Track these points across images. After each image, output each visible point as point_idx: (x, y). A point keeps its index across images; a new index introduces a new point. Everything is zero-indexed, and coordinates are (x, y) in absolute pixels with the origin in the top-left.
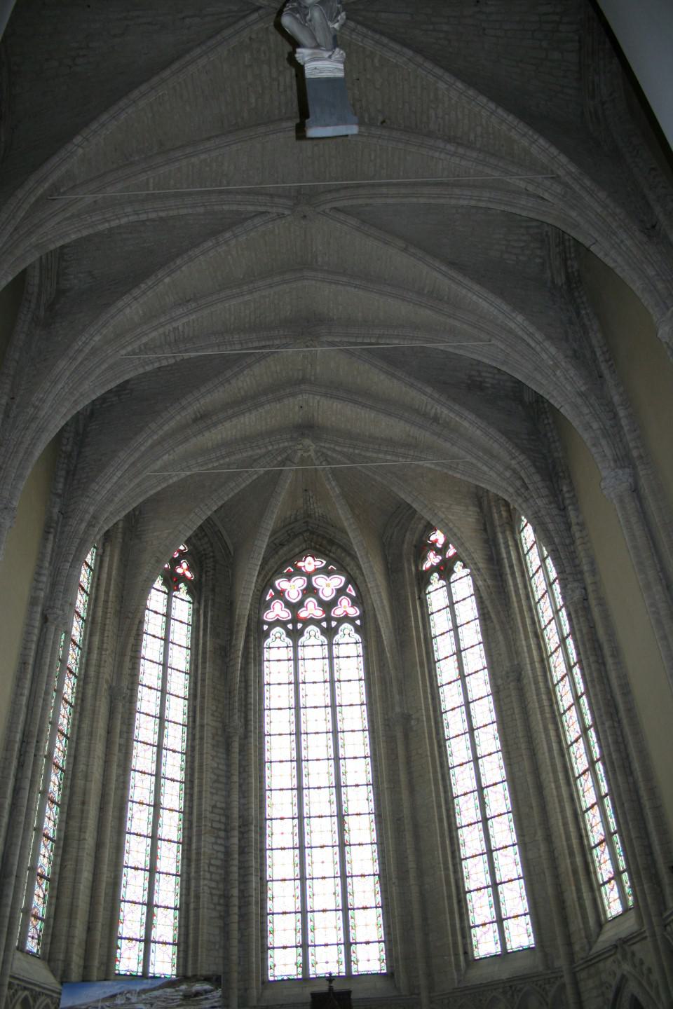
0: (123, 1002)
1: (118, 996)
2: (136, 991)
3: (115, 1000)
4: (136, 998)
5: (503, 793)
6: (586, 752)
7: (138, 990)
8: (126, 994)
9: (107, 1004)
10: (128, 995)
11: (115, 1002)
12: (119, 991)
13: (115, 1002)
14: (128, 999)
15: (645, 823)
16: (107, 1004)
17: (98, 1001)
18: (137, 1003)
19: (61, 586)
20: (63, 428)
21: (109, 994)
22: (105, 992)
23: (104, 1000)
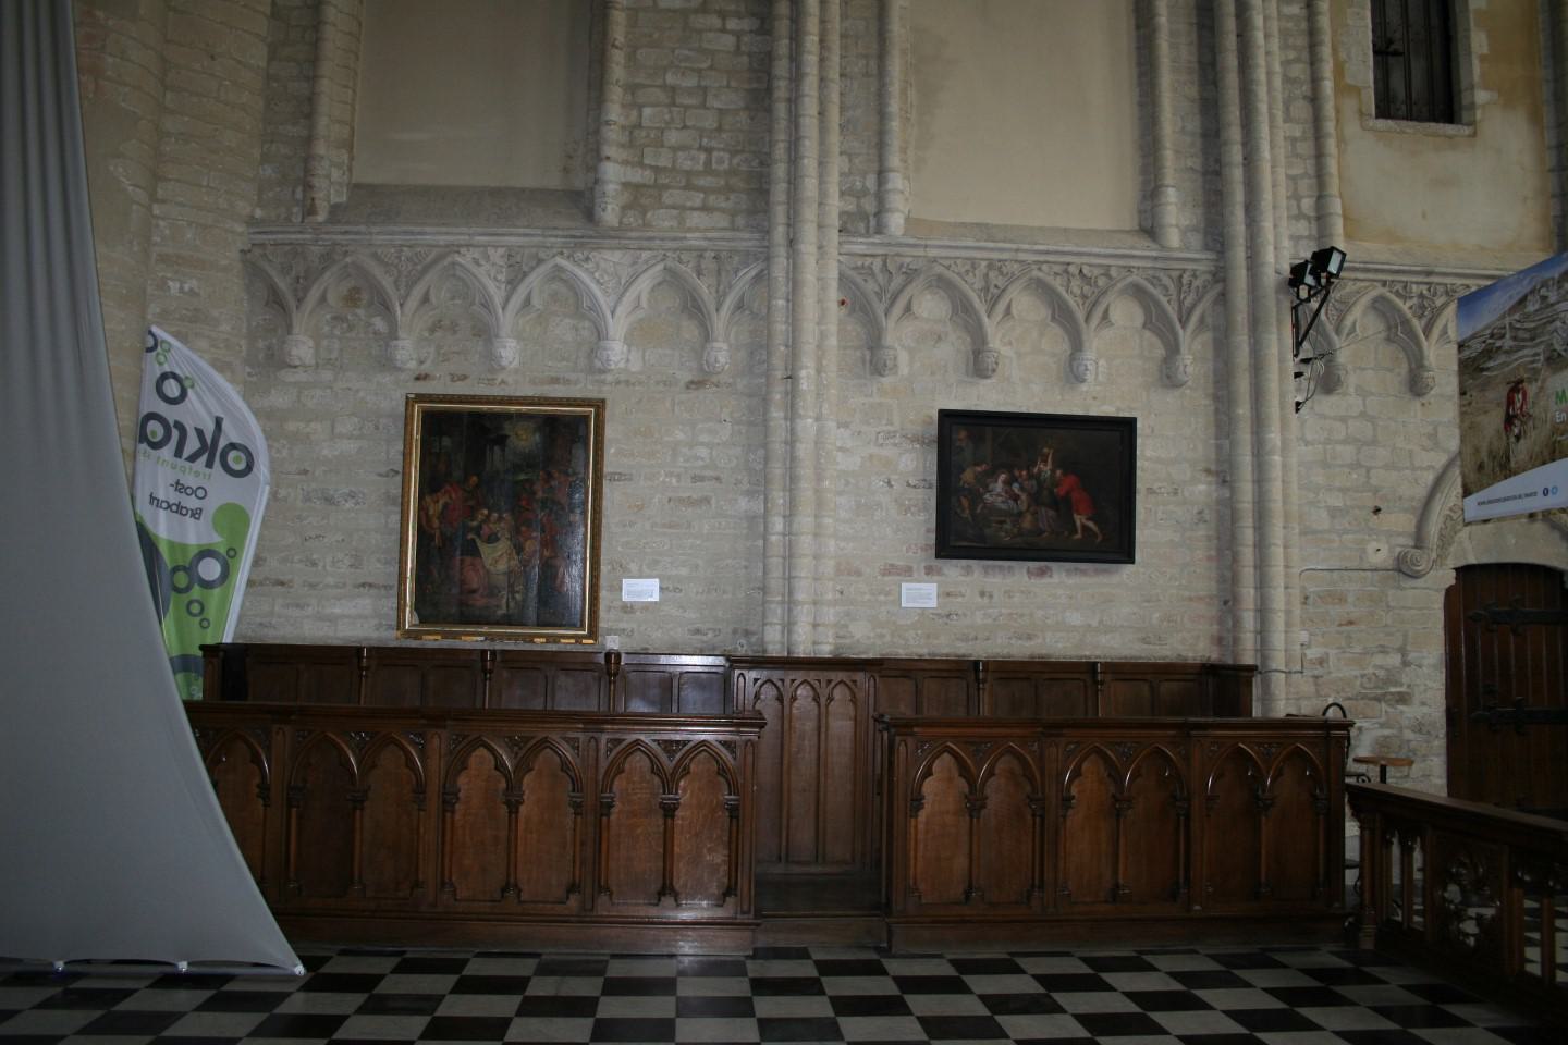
0: (1537, 307)
1: (1529, 298)
2: (1553, 279)
3: (1525, 307)
4: (1555, 293)
5: (1309, 403)
6: (1460, 92)
7: (1557, 276)
8: (1539, 290)
9: (1517, 317)
10: (1543, 292)
11: (1526, 311)
12: (1529, 289)
13: (1526, 311)
14: (1544, 298)
15: (419, 279)
16: (1517, 317)
17: (1503, 317)
18: (1559, 302)
19: (485, 685)
20: (1006, 226)
21: (1516, 299)
22: (1511, 297)
23: (1512, 310)
